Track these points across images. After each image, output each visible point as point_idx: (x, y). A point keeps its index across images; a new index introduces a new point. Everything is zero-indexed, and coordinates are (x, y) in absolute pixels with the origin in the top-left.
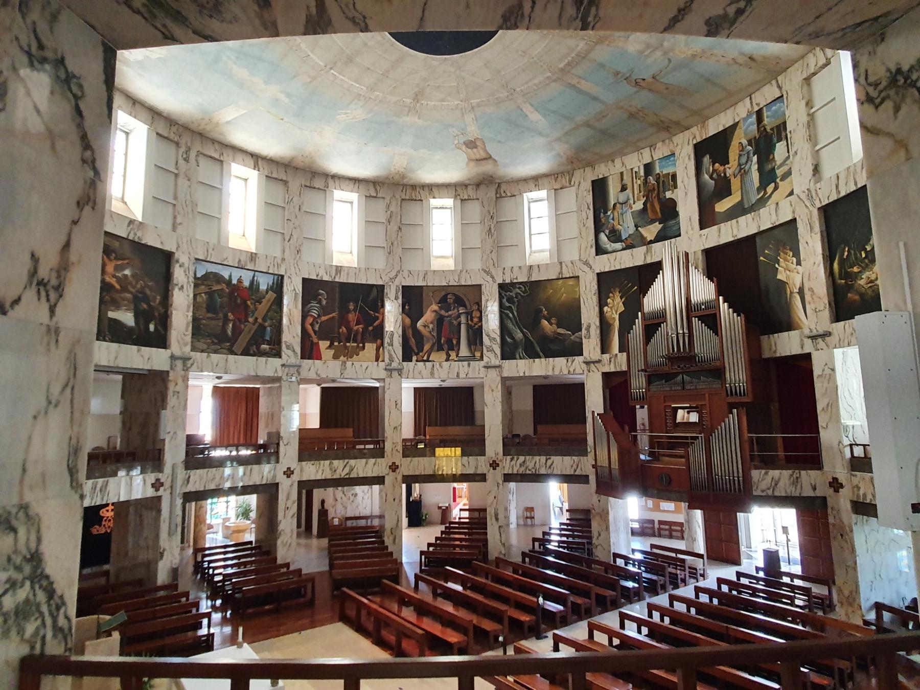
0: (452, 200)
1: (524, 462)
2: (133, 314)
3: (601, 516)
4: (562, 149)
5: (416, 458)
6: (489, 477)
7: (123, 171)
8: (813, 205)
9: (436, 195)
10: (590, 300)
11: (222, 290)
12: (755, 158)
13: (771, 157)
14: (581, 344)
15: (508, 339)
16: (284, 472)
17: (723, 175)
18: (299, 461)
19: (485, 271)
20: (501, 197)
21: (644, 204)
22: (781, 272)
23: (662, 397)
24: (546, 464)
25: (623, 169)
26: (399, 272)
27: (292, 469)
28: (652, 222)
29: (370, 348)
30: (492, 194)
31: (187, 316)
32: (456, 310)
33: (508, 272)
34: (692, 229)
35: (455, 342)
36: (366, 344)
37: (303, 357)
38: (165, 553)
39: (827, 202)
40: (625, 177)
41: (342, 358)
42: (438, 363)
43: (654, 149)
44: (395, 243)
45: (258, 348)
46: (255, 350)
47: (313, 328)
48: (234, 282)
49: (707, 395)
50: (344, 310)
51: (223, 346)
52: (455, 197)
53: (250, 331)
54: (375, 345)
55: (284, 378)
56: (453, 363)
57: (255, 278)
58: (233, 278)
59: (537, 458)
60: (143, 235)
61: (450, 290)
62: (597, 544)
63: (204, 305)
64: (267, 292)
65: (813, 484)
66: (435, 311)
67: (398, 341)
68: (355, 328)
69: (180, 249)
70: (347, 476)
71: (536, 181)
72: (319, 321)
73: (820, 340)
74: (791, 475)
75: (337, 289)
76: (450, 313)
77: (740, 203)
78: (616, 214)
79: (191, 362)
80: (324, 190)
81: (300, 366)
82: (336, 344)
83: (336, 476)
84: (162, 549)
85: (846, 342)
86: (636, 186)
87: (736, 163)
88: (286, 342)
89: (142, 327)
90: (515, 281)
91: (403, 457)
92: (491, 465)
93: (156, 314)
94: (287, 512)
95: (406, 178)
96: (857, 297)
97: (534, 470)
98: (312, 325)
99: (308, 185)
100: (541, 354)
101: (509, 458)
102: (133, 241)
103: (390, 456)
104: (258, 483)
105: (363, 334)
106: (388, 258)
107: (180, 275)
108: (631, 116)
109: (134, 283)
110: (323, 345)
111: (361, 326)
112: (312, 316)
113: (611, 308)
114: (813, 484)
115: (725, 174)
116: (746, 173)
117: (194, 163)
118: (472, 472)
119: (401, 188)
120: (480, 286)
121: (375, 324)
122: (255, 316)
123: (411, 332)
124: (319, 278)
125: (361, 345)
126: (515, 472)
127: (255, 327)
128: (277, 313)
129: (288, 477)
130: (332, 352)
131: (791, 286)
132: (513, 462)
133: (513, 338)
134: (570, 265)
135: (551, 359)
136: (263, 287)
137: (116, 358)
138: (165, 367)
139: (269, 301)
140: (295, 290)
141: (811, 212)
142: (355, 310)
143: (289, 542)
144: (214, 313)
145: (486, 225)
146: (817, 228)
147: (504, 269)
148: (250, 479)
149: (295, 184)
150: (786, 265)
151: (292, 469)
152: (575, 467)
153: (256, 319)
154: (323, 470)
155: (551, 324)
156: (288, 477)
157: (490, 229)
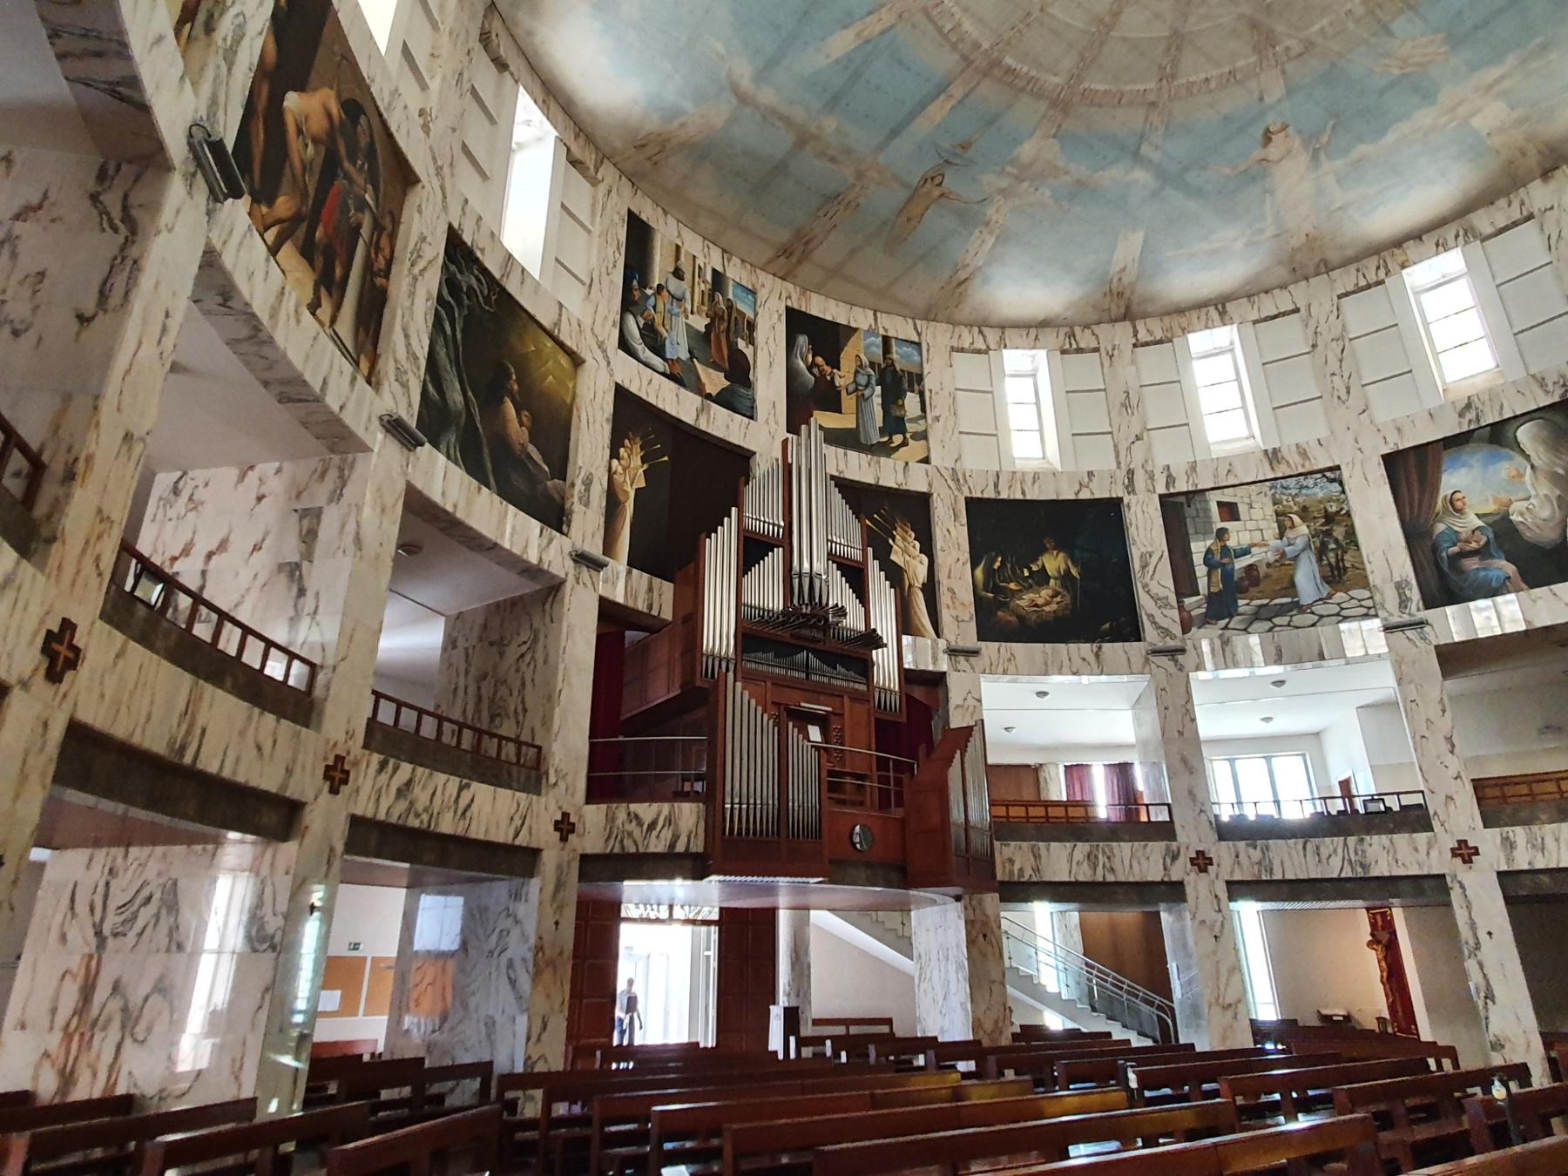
1: (409, 783)
8: (959, 490)
10: (598, 426)
22: (896, 553)
34: (776, 423)
39: (979, 495)
59: (441, 778)
73: (961, 659)
85: (1000, 669)
96: (1013, 619)
97: (425, 817)
100: (492, 480)
101: (376, 758)
118: (274, 790)
132: (384, 777)
152: (518, 822)
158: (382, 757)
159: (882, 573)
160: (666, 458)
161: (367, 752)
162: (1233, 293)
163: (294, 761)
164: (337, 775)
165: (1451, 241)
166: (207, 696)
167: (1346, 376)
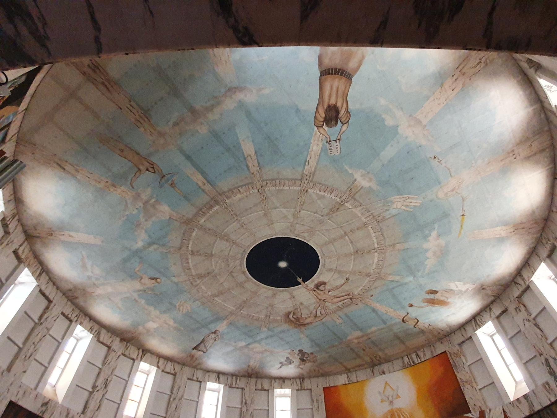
119: (473, 322)
162: (51, 273)
165: (94, 331)
167: (36, 349)
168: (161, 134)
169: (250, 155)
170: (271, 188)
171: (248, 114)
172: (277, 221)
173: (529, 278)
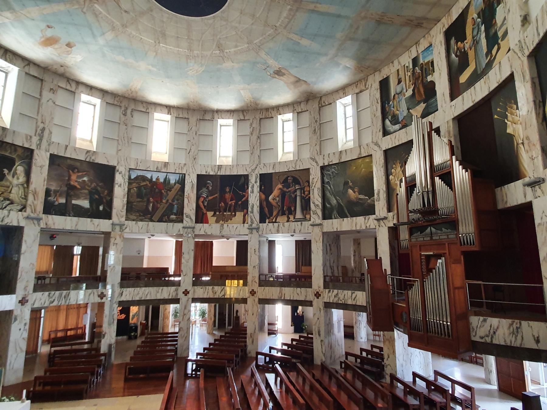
0: (292, 114)
1: (337, 294)
2: (88, 201)
3: (389, 342)
4: (349, 63)
5: (267, 287)
6: (314, 303)
7: (92, 126)
9: (281, 112)
11: (147, 184)
12: (483, 28)
13: (494, 22)
14: (374, 205)
15: (328, 205)
16: (183, 292)
17: (463, 50)
18: (193, 286)
19: (311, 158)
20: (323, 106)
21: (413, 90)
23: (419, 246)
24: (351, 296)
25: (399, 67)
26: (257, 165)
27: (188, 291)
28: (419, 103)
29: (239, 215)
30: (316, 105)
31: (123, 201)
32: (294, 187)
33: (326, 158)
34: (445, 103)
35: (293, 209)
36: (237, 213)
37: (197, 222)
38: (106, 335)
40: (400, 73)
41: (221, 222)
42: (282, 224)
43: (419, 45)
44: (256, 147)
45: (168, 218)
46: (167, 219)
47: (203, 204)
48: (154, 180)
49: (447, 245)
50: (223, 192)
51: (146, 217)
52: (293, 112)
53: (164, 207)
54: (242, 213)
55: (185, 235)
56: (291, 223)
57: (168, 177)
58: (153, 177)
59: (346, 292)
60: (95, 158)
61: (289, 174)
62: (387, 364)
63: (135, 194)
64: (175, 184)
65: (536, 336)
66: (280, 189)
67: (256, 209)
68: (230, 203)
69: (119, 164)
70: (223, 297)
71: (343, 90)
72: (207, 200)
74: (511, 325)
75: (219, 179)
76: (289, 189)
77: (475, 71)
78: (395, 103)
79: (125, 226)
80: (212, 119)
81: (194, 228)
82: (218, 213)
83: (217, 296)
84: (104, 333)
86: (407, 78)
87: (471, 37)
88: (186, 213)
89: (94, 208)
90: (331, 163)
91: (259, 286)
92: (315, 295)
93: (105, 201)
94: (185, 317)
95: (259, 104)
97: (343, 301)
98: (203, 202)
99: (202, 118)
100: (348, 214)
101: (327, 290)
102: (89, 162)
103: (250, 285)
104: (167, 298)
105: (235, 206)
106: (251, 157)
107: (118, 178)
108: (379, 22)
109: (89, 184)
110: (210, 214)
111: (234, 201)
112: (203, 197)
113: (394, 177)
114: (536, 336)
115: (464, 49)
116: (477, 43)
117: (130, 116)
118: (303, 300)
120: (309, 169)
121: (242, 200)
122: (167, 198)
123: (265, 203)
124: (207, 174)
125: (233, 213)
126: (331, 301)
127: (167, 205)
128: (181, 196)
129: (186, 295)
130: (215, 218)
131: (517, 139)
132: (330, 294)
133: (330, 204)
134: (366, 147)
135: (354, 218)
136: (172, 182)
137: (76, 225)
138: (109, 230)
139: (176, 189)
140: (192, 182)
141: (522, 62)
142: (230, 192)
143: (186, 335)
144: (141, 198)
145: (313, 127)
146: (528, 77)
147: (324, 156)
148: (161, 295)
149: (193, 120)
150: (513, 118)
151: (188, 291)
153: (168, 200)
154: (208, 292)
155: (354, 192)
156: (186, 295)
157: (315, 129)
158: (329, 290)
159: (461, 166)
160: (498, 109)
161: (325, 290)
163: (307, 295)
164: (318, 295)
166: (283, 290)
168: (365, 18)
169: (301, 40)
170: (270, 32)
171: (319, 54)
172: (241, 17)
173: (82, 92)
